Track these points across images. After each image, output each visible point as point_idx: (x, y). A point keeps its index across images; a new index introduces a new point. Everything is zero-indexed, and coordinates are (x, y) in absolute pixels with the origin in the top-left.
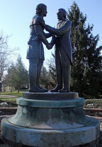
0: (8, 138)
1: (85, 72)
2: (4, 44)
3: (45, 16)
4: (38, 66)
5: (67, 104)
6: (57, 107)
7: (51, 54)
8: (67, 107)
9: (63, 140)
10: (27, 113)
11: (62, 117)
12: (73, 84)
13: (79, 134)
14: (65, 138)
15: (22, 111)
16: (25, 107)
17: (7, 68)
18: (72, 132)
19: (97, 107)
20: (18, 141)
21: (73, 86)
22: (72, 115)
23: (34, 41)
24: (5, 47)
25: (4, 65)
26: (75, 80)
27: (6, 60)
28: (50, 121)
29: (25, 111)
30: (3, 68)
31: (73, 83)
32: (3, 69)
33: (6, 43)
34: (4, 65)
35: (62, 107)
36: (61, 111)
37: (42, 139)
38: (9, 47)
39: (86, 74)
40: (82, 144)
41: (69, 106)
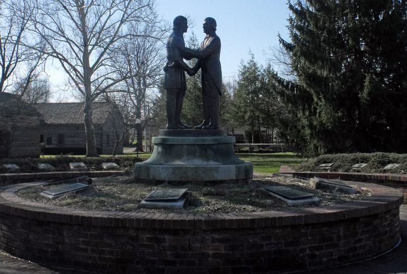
0: (141, 177)
1: (366, 91)
2: (143, 9)
3: (186, 32)
4: (177, 98)
5: (203, 140)
6: (192, 143)
7: (278, 38)
8: (203, 143)
9: (194, 173)
10: (162, 152)
11: (197, 154)
12: (331, 123)
13: (211, 169)
14: (196, 172)
15: (158, 149)
16: (160, 146)
17: (162, 68)
18: (204, 166)
19: (335, 170)
20: (151, 177)
21: (333, 127)
22: (210, 152)
23: (171, 67)
24: (146, 19)
25: (148, 72)
26: (337, 112)
27: (154, 54)
28: (185, 157)
29: (160, 149)
30: (144, 78)
31: (331, 120)
32: (145, 82)
33: (148, 5)
34: (147, 70)
35: (198, 143)
36: (197, 147)
37: (173, 173)
38: (159, 19)
39: (369, 94)
40: (215, 180)
41: (206, 143)
